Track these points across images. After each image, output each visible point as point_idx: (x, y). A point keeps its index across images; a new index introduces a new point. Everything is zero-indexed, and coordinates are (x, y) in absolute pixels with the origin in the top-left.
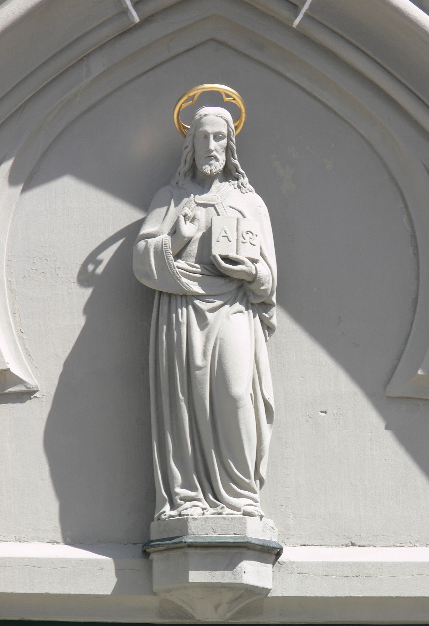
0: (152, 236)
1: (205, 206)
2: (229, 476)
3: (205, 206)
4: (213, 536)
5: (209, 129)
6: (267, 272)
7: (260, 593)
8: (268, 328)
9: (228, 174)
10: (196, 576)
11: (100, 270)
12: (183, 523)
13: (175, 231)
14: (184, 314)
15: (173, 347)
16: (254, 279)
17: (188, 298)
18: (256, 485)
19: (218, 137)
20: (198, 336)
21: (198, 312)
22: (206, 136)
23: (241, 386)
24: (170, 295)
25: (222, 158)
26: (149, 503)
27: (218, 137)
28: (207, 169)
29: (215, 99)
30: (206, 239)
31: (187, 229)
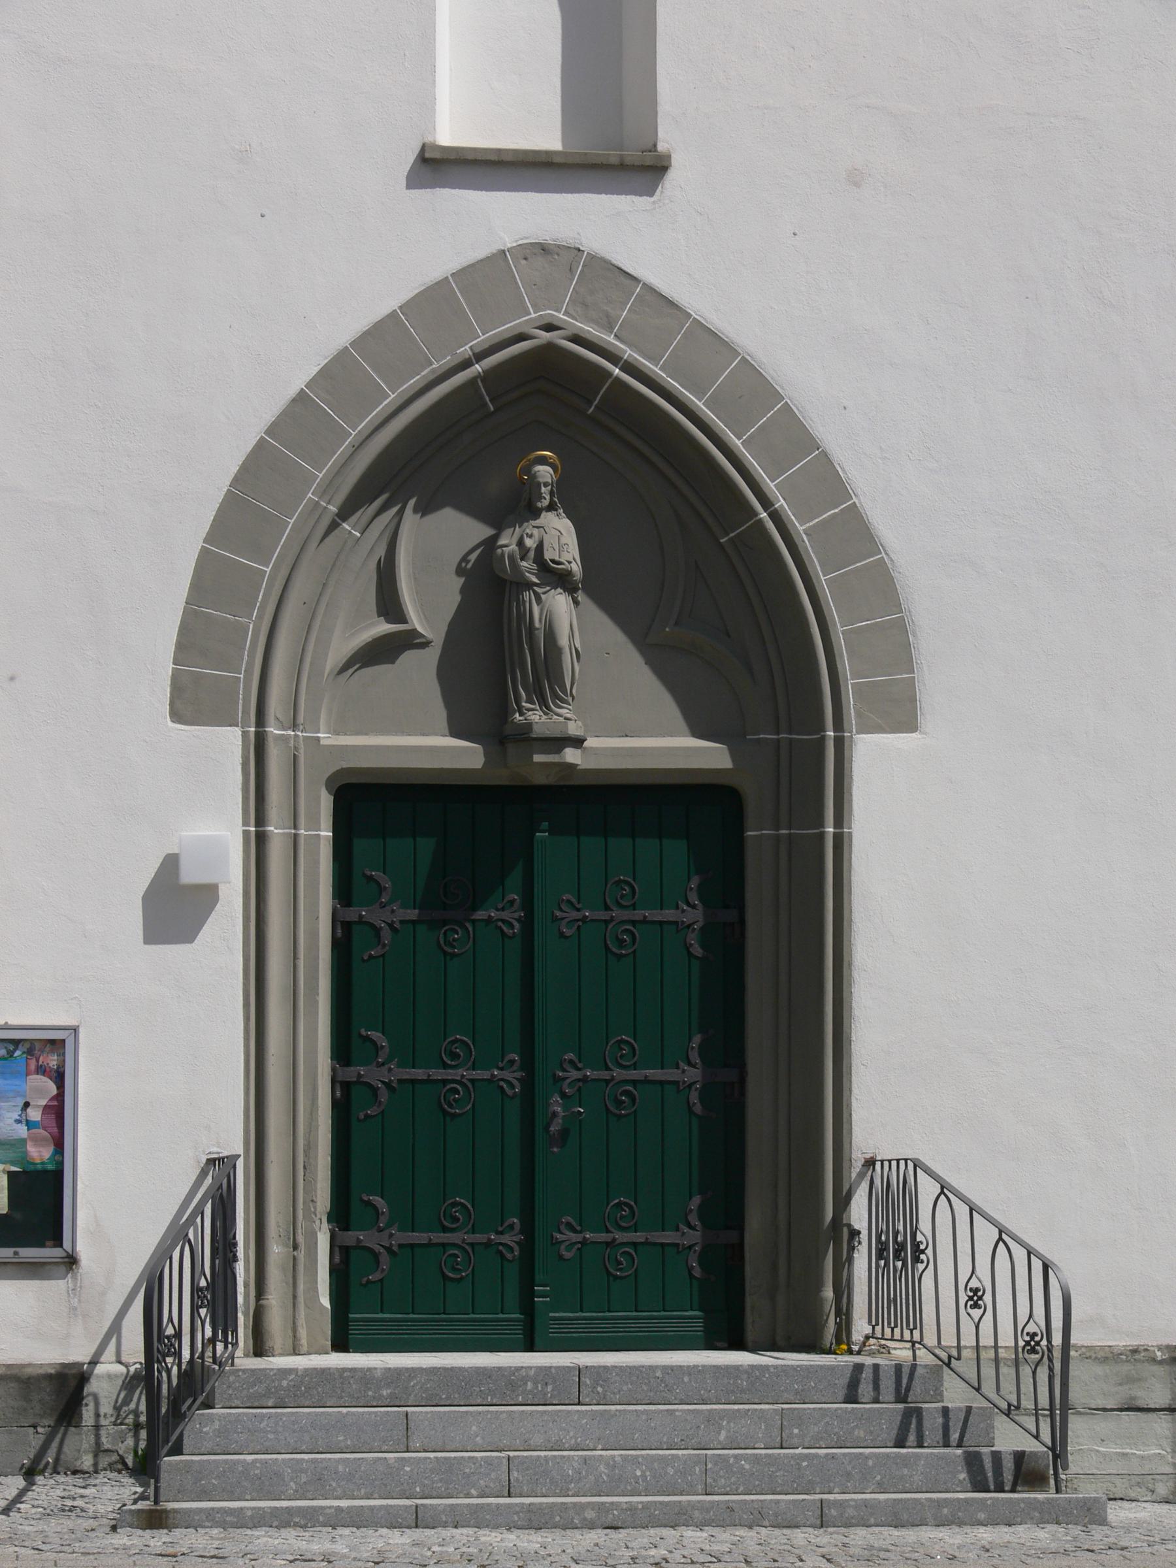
0: (506, 546)
1: (538, 527)
2: (556, 696)
3: (538, 527)
4: (548, 733)
5: (541, 480)
6: (576, 568)
7: (572, 766)
8: (576, 603)
9: (551, 507)
10: (538, 758)
11: (469, 566)
12: (529, 726)
13: (520, 543)
14: (526, 595)
15: (521, 616)
16: (569, 573)
17: (529, 586)
18: (570, 699)
19: (546, 485)
20: (536, 609)
21: (536, 594)
22: (539, 484)
23: (563, 641)
24: (517, 584)
25: (548, 497)
26: (504, 713)
27: (546, 485)
28: (539, 505)
29: (543, 461)
30: (540, 547)
31: (529, 542)
